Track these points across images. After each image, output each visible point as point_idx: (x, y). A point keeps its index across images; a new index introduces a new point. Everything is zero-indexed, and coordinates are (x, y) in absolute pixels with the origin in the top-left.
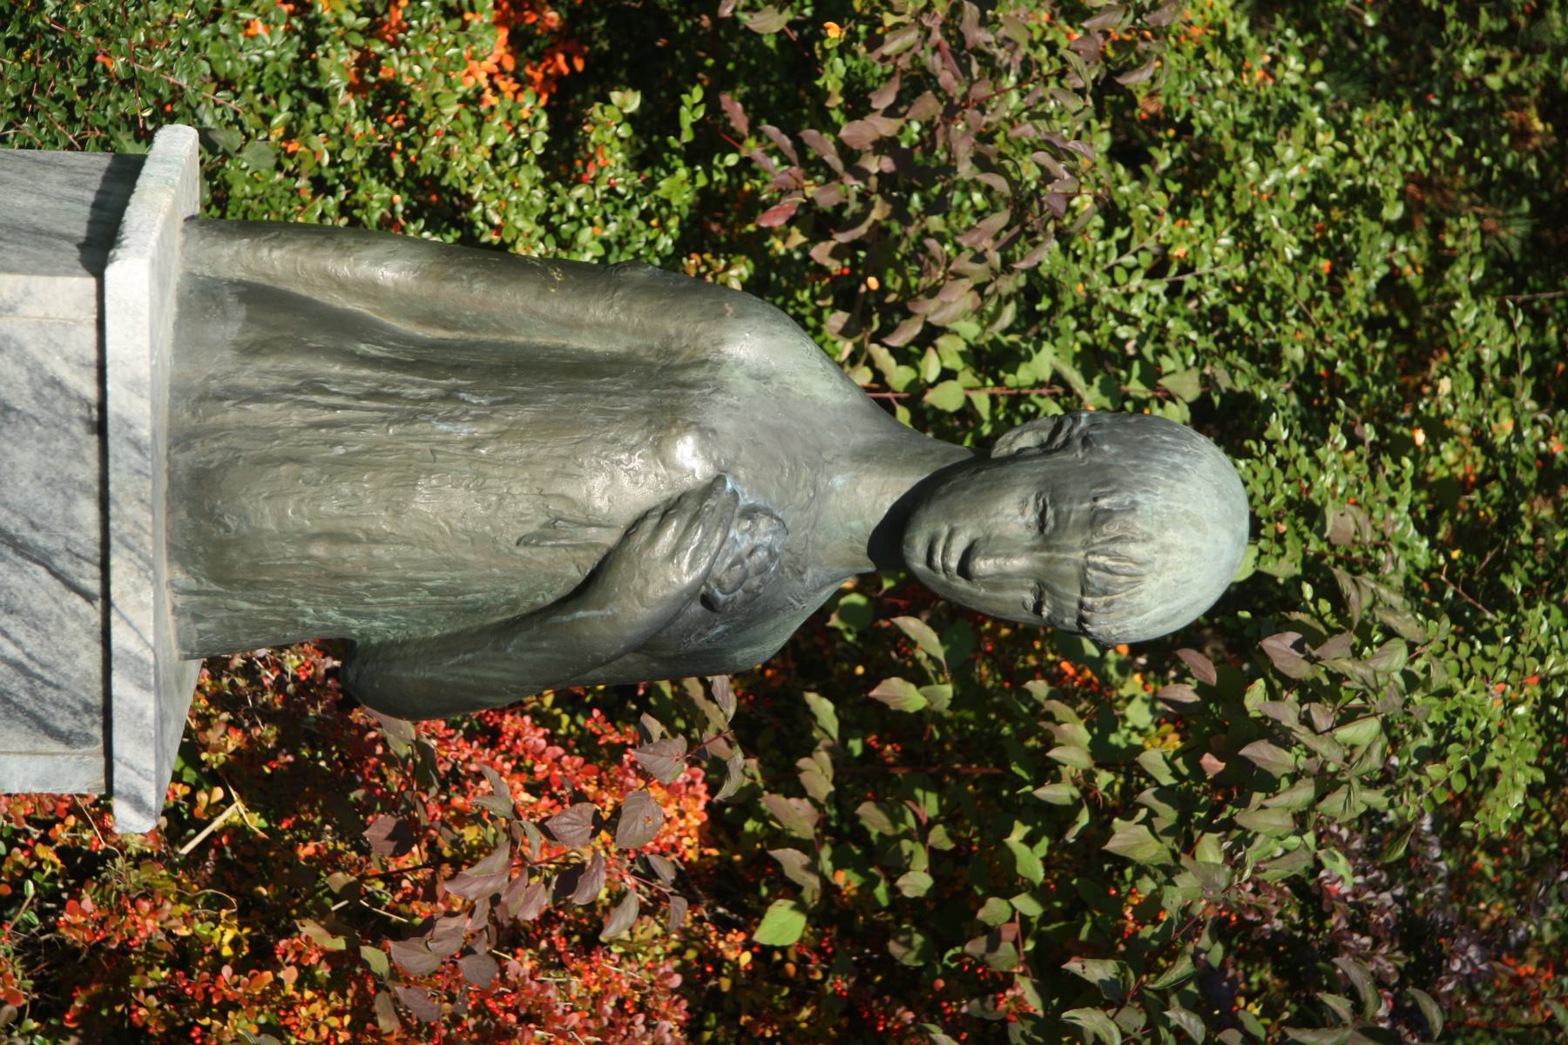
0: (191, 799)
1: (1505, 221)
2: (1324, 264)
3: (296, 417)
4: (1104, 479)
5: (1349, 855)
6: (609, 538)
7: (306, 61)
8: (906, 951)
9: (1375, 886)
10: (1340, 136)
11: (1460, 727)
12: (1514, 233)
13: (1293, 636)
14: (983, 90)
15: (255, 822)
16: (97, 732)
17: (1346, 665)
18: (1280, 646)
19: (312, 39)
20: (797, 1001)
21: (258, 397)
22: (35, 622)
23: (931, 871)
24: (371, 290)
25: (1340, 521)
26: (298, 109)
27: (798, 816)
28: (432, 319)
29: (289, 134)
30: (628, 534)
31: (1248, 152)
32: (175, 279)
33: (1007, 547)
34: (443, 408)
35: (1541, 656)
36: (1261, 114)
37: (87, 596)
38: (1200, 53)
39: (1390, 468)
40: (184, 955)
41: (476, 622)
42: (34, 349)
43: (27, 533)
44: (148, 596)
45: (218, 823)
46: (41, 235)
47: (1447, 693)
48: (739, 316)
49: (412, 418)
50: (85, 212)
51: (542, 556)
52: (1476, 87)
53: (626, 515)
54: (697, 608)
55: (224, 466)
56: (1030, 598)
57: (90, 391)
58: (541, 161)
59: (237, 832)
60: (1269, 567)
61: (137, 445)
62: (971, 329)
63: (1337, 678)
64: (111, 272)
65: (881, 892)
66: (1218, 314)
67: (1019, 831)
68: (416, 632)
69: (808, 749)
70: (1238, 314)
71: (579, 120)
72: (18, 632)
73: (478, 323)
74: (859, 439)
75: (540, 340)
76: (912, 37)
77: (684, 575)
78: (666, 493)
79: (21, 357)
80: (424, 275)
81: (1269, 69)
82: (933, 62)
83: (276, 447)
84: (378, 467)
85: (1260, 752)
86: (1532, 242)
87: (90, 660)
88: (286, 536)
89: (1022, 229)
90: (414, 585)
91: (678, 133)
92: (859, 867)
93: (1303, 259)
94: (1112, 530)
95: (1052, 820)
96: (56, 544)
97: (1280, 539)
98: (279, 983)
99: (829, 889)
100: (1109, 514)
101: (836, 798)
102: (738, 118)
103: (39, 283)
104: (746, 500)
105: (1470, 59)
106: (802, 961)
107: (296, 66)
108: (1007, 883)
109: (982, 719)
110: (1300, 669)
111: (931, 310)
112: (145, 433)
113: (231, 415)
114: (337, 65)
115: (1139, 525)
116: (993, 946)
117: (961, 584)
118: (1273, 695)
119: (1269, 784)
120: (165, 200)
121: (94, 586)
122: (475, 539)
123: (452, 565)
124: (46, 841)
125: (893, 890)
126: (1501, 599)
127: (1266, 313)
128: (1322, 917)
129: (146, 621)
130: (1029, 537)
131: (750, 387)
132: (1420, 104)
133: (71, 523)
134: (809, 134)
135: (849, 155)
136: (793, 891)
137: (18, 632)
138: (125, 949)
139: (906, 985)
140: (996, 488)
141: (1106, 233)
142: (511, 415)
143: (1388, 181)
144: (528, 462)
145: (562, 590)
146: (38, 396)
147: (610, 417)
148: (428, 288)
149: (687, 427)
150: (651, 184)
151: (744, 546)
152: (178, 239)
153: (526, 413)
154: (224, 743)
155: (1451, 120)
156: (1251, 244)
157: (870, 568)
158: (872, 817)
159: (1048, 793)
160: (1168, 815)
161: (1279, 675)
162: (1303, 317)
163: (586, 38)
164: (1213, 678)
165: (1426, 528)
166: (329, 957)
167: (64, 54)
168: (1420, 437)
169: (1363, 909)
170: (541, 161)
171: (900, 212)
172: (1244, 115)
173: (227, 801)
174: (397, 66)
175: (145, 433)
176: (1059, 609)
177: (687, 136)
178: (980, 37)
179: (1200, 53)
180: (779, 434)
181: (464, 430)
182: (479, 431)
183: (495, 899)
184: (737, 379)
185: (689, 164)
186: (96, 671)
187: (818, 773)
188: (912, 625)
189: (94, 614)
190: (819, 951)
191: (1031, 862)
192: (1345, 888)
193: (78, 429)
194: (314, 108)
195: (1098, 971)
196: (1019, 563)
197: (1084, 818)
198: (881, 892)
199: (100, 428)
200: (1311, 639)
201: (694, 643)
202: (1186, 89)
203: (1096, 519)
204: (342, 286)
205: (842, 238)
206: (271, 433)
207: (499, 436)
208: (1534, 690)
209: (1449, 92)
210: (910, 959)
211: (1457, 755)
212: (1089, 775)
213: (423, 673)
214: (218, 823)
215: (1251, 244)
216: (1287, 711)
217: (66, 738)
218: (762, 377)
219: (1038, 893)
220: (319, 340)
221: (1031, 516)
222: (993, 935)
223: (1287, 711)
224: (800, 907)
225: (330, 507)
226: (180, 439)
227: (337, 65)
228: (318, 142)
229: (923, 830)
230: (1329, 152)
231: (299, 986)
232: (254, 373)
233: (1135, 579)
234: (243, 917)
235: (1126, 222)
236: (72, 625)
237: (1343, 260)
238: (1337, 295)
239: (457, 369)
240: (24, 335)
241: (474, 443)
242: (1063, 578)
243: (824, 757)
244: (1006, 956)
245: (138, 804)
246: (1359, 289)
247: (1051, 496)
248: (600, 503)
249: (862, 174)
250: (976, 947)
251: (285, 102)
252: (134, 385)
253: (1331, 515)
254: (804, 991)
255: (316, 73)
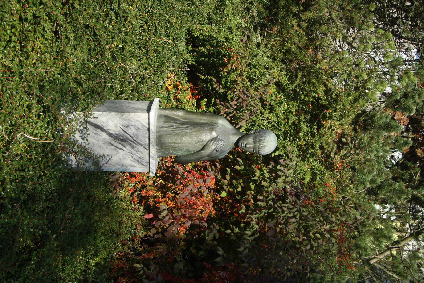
0: (156, 179)
1: (307, 116)
2: (286, 120)
3: (170, 130)
4: (261, 136)
5: (289, 186)
6: (205, 143)
7: (168, 96)
8: (238, 197)
9: (292, 190)
10: (288, 105)
11: (302, 171)
12: (308, 118)
13: (283, 160)
14: (246, 99)
15: (163, 182)
16: (148, 165)
17: (289, 163)
18: (281, 161)
19: (169, 94)
20: (226, 204)
21: (166, 127)
22: (141, 153)
23: (241, 188)
24: (178, 116)
25: (288, 148)
26: (168, 101)
27: (226, 182)
28: (185, 119)
29: (167, 104)
30: (207, 143)
31: (277, 107)
32: (157, 114)
33: (250, 144)
34: (187, 129)
35: (311, 163)
36: (279, 102)
37: (147, 150)
38: (272, 95)
39: (294, 142)
40: (155, 197)
41: (191, 153)
42: (142, 122)
43: (141, 142)
44: (154, 149)
45: (159, 182)
46: (142, 109)
47: (300, 167)
48: (220, 118)
49: (183, 130)
50: (147, 107)
51: (198, 145)
52: (304, 100)
53: (207, 140)
54: (215, 151)
55: (162, 135)
56: (253, 150)
57: (148, 126)
58: (195, 107)
59: (161, 183)
60: (280, 153)
61: (153, 132)
62: (245, 127)
63: (288, 165)
64: (150, 113)
65: (235, 191)
66: (274, 126)
67: (251, 183)
68: (183, 154)
69: (227, 174)
70: (276, 125)
71: (200, 102)
72: (140, 154)
73: (190, 119)
74: (233, 132)
75: (197, 121)
76: (238, 92)
77: (213, 147)
78: (212, 138)
79: (140, 123)
80: (184, 114)
81: (280, 97)
82: (241, 95)
83: (168, 133)
84: (179, 135)
85: (279, 173)
86: (310, 118)
87: (147, 157)
88: (169, 143)
89: (251, 114)
90: (183, 148)
91: (211, 103)
92: (233, 188)
93: (284, 119)
94: (262, 142)
95: (255, 182)
96: (144, 144)
97: (281, 150)
98: (166, 200)
99: (229, 191)
100: (262, 140)
101: (230, 180)
102: (219, 102)
103: (142, 114)
104: (220, 139)
105: (303, 97)
106: (226, 199)
107: (167, 96)
108: (250, 190)
109: (247, 172)
110: (284, 164)
111: (241, 124)
112: (154, 131)
113: (163, 129)
114: (172, 97)
115: (265, 141)
116: (249, 196)
117: (245, 148)
118: (280, 166)
119: (280, 177)
120: (156, 105)
121: (148, 148)
122: (190, 143)
123: (187, 146)
124: (140, 184)
125: (237, 191)
126: (306, 157)
127: (280, 126)
128: (286, 193)
129: (153, 152)
130: (253, 143)
131: (221, 126)
132: (297, 102)
133: (145, 141)
134: (227, 103)
135: (231, 106)
136: (225, 191)
137: (140, 154)
138: (149, 196)
139: (238, 201)
140: (249, 137)
141: (261, 116)
142: (194, 129)
143: (294, 110)
144: (196, 134)
145: (200, 149)
146: (142, 127)
147: (205, 129)
148: (185, 115)
149: (214, 131)
150: (208, 109)
151: (220, 144)
152: (157, 110)
153: (196, 129)
154: (160, 173)
155: (300, 103)
156: (278, 117)
157: (234, 147)
158: (234, 182)
159: (255, 178)
160: (268, 181)
161: (281, 164)
162: (284, 126)
163: (200, 94)
164: (274, 165)
165: (299, 150)
166: (172, 196)
167: (142, 94)
168: (298, 140)
169: (291, 192)
170: (195, 107)
171: (237, 113)
172: (277, 102)
173: (160, 180)
174: (179, 96)
175: (154, 131)
176: (256, 151)
177: (212, 104)
178: (246, 93)
179: (272, 95)
180: (224, 131)
181: (189, 131)
182: (190, 131)
183: (191, 190)
184: (219, 125)
185: (213, 107)
186: (148, 158)
187: (228, 177)
188: (239, 159)
189: (148, 151)
190: (228, 198)
191: (253, 187)
192: (289, 190)
193: (146, 131)
194: (169, 101)
195: (261, 198)
196: (251, 146)
197: (259, 181)
198: (235, 191)
199: (149, 130)
200: (285, 160)
201: (215, 155)
202: (270, 99)
203: (260, 141)
204: (175, 115)
205: (230, 115)
206: (167, 131)
207: (193, 131)
208: (310, 167)
209: (300, 101)
210: (239, 198)
211: (301, 174)
212: (259, 176)
213: (184, 159)
214: (159, 182)
215: (278, 117)
216: (282, 168)
217: (145, 166)
218: (222, 125)
219: (253, 190)
220: (173, 121)
221: (253, 140)
222: (249, 196)
223: (282, 168)
224: (226, 192)
225: (174, 140)
226: (157, 132)
227: (172, 97)
228: (170, 105)
229: (240, 184)
230: (287, 107)
231: (169, 200)
232: (165, 125)
233: (265, 147)
234: (162, 193)
235: (263, 114)
236: (145, 153)
237: (288, 119)
238: (288, 123)
239: (188, 124)
240: (141, 120)
241: (190, 132)
242: (257, 147)
243: (229, 175)
244: (250, 198)
245: (153, 173)
246: (290, 122)
247: (255, 138)
248: (204, 139)
249: (233, 108)
250: (247, 197)
251: (166, 101)
252: (153, 125)
253: (287, 147)
254: (226, 203)
255: (169, 97)
